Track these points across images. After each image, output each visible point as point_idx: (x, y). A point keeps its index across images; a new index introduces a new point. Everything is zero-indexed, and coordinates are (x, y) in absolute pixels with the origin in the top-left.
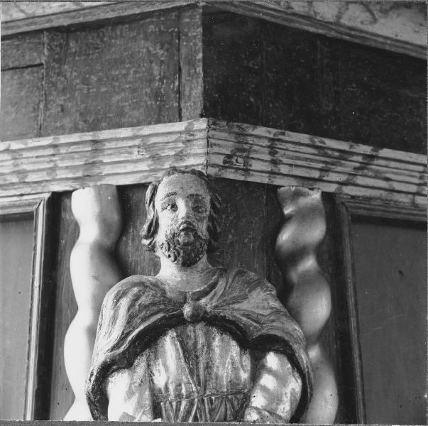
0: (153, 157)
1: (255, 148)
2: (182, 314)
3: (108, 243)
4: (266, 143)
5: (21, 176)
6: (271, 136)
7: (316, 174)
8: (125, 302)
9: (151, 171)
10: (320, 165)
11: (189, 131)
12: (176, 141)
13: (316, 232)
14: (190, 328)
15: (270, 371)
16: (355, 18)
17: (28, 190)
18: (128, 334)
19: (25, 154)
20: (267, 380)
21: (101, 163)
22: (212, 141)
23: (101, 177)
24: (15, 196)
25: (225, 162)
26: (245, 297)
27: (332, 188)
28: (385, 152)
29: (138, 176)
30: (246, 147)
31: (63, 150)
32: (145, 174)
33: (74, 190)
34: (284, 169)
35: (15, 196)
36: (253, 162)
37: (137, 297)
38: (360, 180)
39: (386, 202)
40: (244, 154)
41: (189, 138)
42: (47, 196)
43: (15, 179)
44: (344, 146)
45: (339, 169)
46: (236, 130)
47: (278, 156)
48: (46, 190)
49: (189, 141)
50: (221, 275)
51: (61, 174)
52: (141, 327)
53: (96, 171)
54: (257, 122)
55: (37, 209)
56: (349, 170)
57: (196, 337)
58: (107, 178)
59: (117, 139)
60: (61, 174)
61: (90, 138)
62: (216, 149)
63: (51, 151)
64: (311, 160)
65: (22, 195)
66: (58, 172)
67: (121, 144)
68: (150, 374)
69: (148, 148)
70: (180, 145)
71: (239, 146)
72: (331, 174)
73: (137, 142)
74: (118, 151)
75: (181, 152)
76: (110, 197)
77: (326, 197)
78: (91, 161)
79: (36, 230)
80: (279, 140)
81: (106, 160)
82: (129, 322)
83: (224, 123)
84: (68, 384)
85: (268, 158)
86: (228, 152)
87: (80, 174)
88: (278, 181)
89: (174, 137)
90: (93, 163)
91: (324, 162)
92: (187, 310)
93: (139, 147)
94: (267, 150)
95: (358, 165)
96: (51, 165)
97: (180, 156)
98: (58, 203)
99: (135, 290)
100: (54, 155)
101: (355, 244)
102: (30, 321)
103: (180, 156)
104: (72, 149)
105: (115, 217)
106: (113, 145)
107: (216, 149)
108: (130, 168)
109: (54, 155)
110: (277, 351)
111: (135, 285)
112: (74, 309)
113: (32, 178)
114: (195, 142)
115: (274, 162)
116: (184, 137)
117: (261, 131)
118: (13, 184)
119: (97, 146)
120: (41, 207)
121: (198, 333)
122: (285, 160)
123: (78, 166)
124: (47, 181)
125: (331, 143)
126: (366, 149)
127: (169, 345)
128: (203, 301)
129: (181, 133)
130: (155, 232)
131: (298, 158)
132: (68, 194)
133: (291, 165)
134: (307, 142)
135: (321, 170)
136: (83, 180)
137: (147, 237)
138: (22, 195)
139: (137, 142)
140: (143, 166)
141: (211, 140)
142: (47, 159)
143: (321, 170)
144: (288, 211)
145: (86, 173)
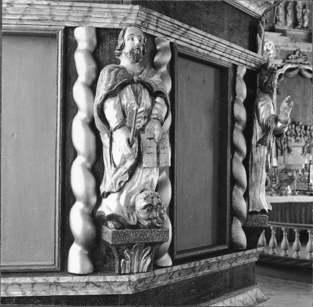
0: (113, 18)
1: (152, 20)
2: (133, 80)
3: (92, 49)
4: (156, 18)
5: (52, 17)
6: (158, 16)
7: (169, 34)
8: (113, 73)
9: (112, 23)
10: (171, 30)
11: (131, 9)
12: (125, 12)
13: (167, 58)
14: (135, 85)
15: (158, 103)
16: (246, 4)
17: (54, 24)
18: (115, 85)
19: (56, 8)
20: (157, 106)
21: (91, 16)
22: (139, 15)
23: (89, 22)
24: (47, 25)
25: (141, 24)
26: (153, 76)
27: (173, 40)
28: (193, 29)
29: (106, 24)
30: (150, 19)
31: (74, 9)
32: (108, 24)
33: (76, 27)
34: (159, 30)
35: (47, 25)
36: (150, 25)
37: (118, 72)
38: (182, 39)
39: (189, 49)
40: (148, 22)
41: (131, 12)
42: (63, 28)
43: (49, 18)
44: (180, 24)
45: (177, 33)
46: (148, 11)
47: (158, 25)
48: (62, 25)
49: (130, 13)
50: (144, 68)
51: (71, 19)
52: (120, 83)
53: (87, 19)
54: (155, 10)
55: (58, 33)
56: (180, 34)
57: (137, 88)
58: (91, 24)
59: (100, 8)
60: (71, 19)
61: (89, 6)
62: (139, 18)
63: (69, 8)
64: (169, 28)
65: (51, 26)
66: (70, 18)
67: (101, 10)
68: (120, 101)
69: (112, 13)
70: (126, 14)
71: (147, 18)
72: (174, 35)
73: (108, 10)
74: (100, 13)
75: (126, 17)
76: (93, 31)
77: (171, 43)
78: (86, 15)
79: (58, 42)
80: (161, 18)
81: (93, 16)
82: (116, 80)
83: (144, 8)
84: (75, 104)
85: (155, 24)
86: (143, 20)
87: (80, 20)
88: (156, 35)
89: (125, 11)
90: (87, 16)
91: (173, 30)
92: (135, 78)
93: (108, 12)
94: (155, 21)
95: (183, 32)
96: (67, 14)
97: (125, 19)
98: (69, 31)
99: (117, 69)
100: (69, 10)
101: (180, 62)
102: (57, 80)
103: (125, 19)
104: (78, 9)
105: (95, 41)
106: (97, 10)
107: (139, 18)
108: (103, 21)
109: (69, 10)
110: (161, 97)
111: (116, 67)
112: (76, 76)
113: (58, 19)
114: (132, 14)
115: (157, 27)
116: (128, 11)
117: (156, 13)
118: (47, 20)
119: (91, 9)
120: (60, 32)
121: (138, 87)
122: (160, 26)
123: (79, 17)
124: (64, 21)
125: (176, 22)
126: (186, 26)
127: (128, 90)
128: (140, 76)
129: (127, 9)
130: (123, 48)
131: (165, 26)
132: (73, 28)
133: (162, 29)
134: (169, 20)
135: (171, 32)
136: (81, 23)
137: (119, 50)
138: (51, 26)
139: (108, 10)
140: (108, 21)
141: (139, 15)
142: (66, 11)
143: (171, 32)
144: (158, 47)
145: (83, 20)
